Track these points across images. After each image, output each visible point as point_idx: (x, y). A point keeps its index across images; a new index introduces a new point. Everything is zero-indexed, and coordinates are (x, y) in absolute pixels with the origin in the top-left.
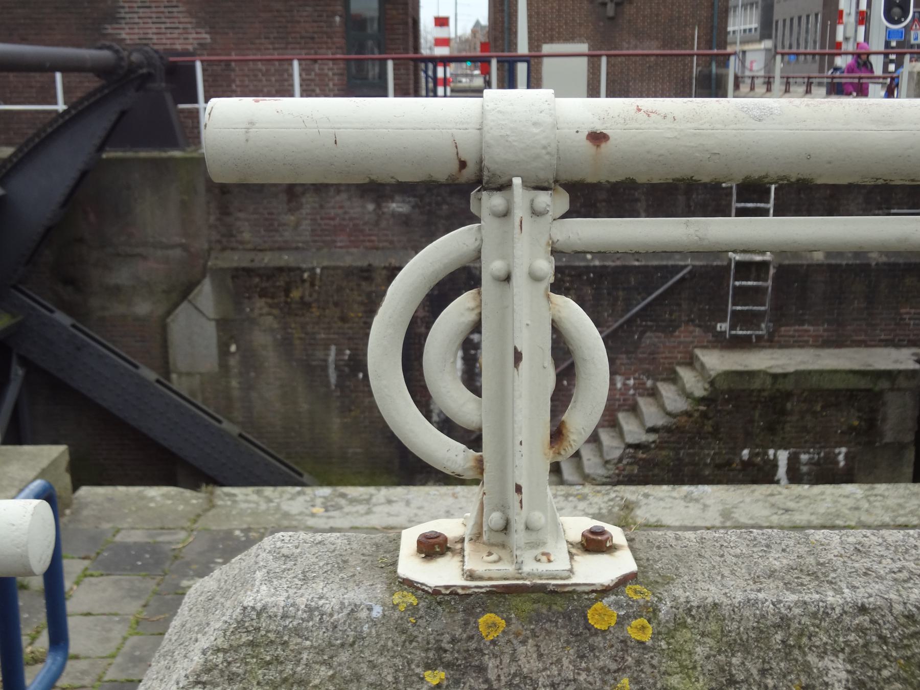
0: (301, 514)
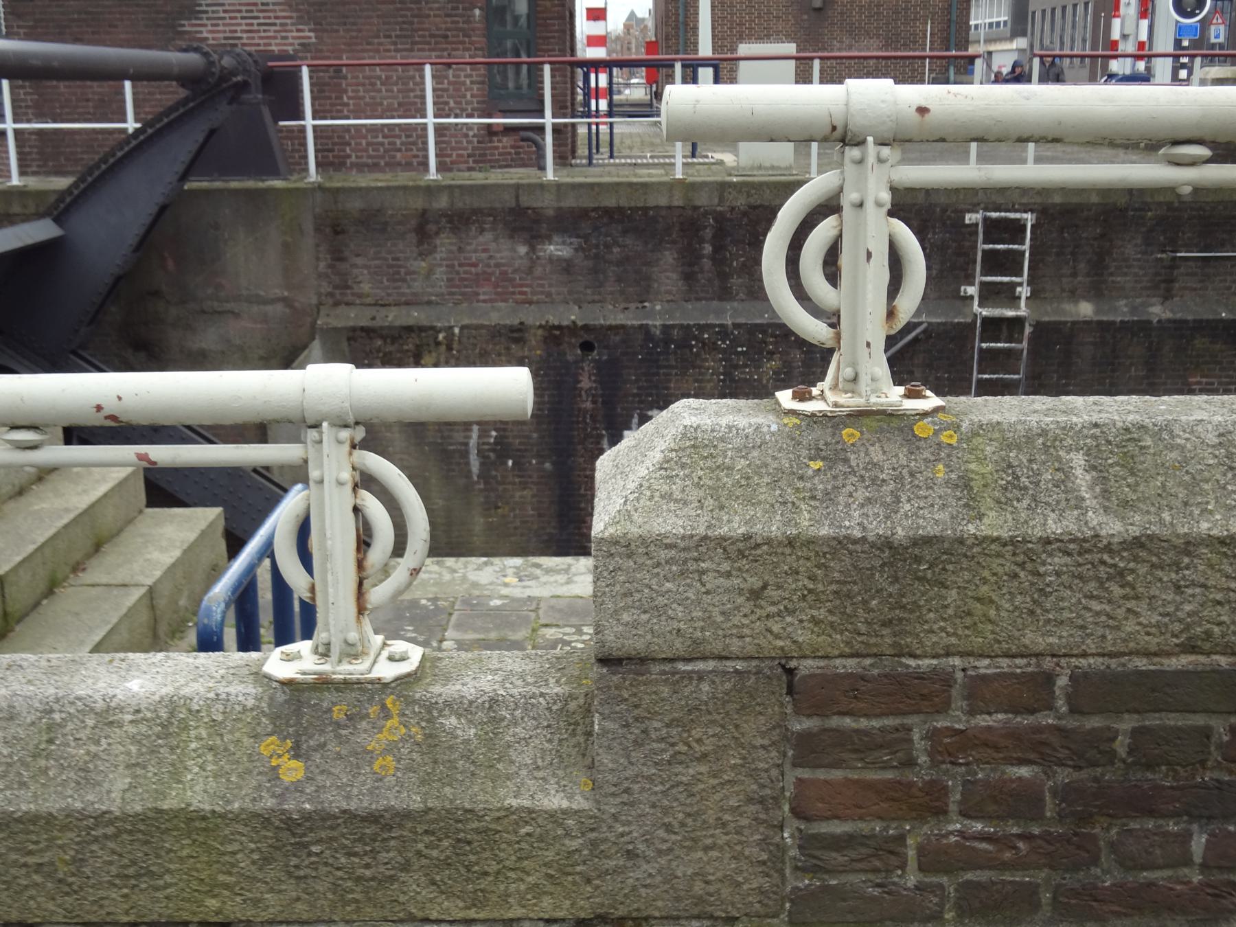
0: (491, 584)
